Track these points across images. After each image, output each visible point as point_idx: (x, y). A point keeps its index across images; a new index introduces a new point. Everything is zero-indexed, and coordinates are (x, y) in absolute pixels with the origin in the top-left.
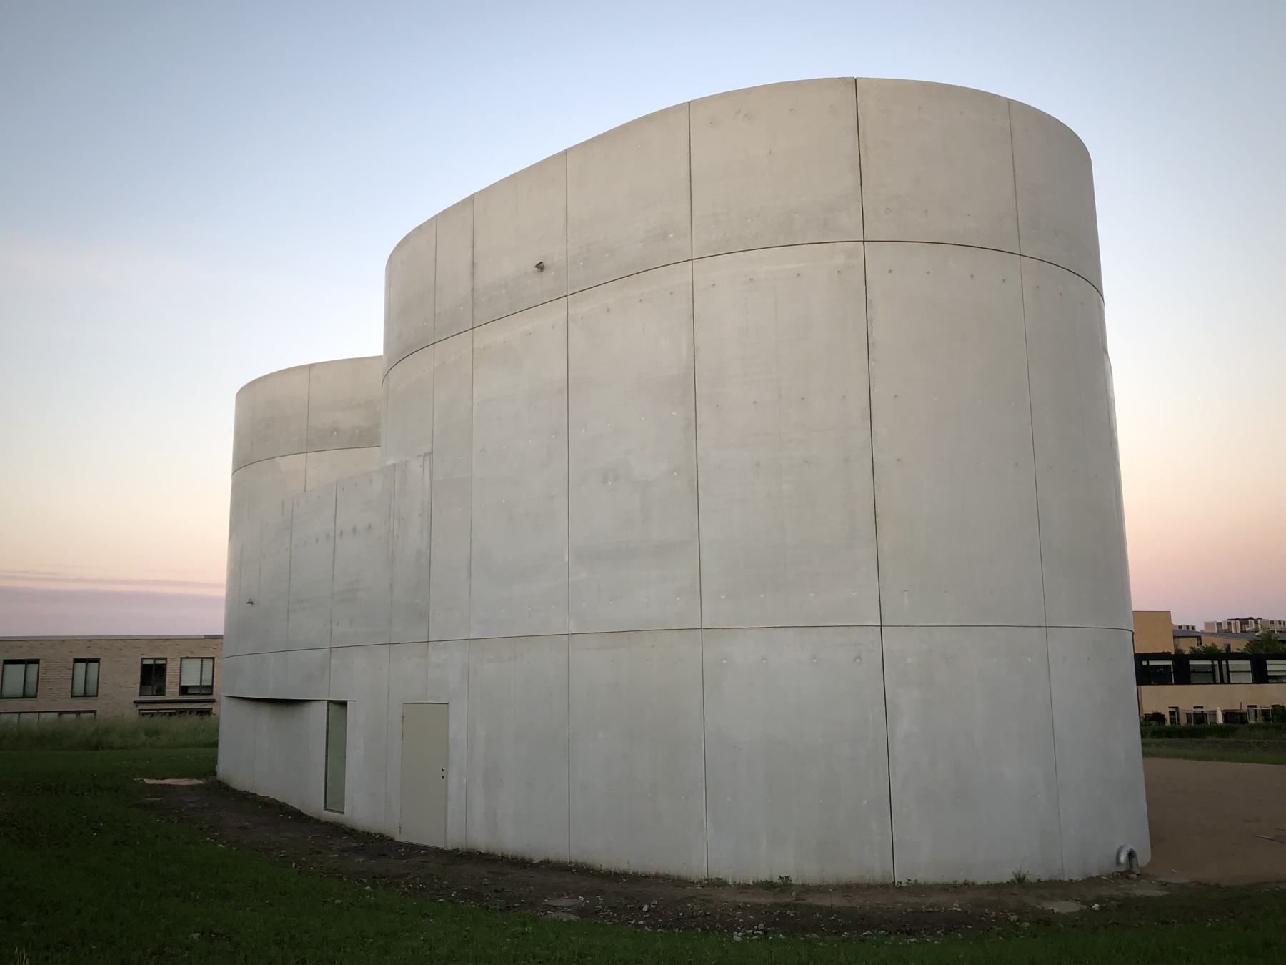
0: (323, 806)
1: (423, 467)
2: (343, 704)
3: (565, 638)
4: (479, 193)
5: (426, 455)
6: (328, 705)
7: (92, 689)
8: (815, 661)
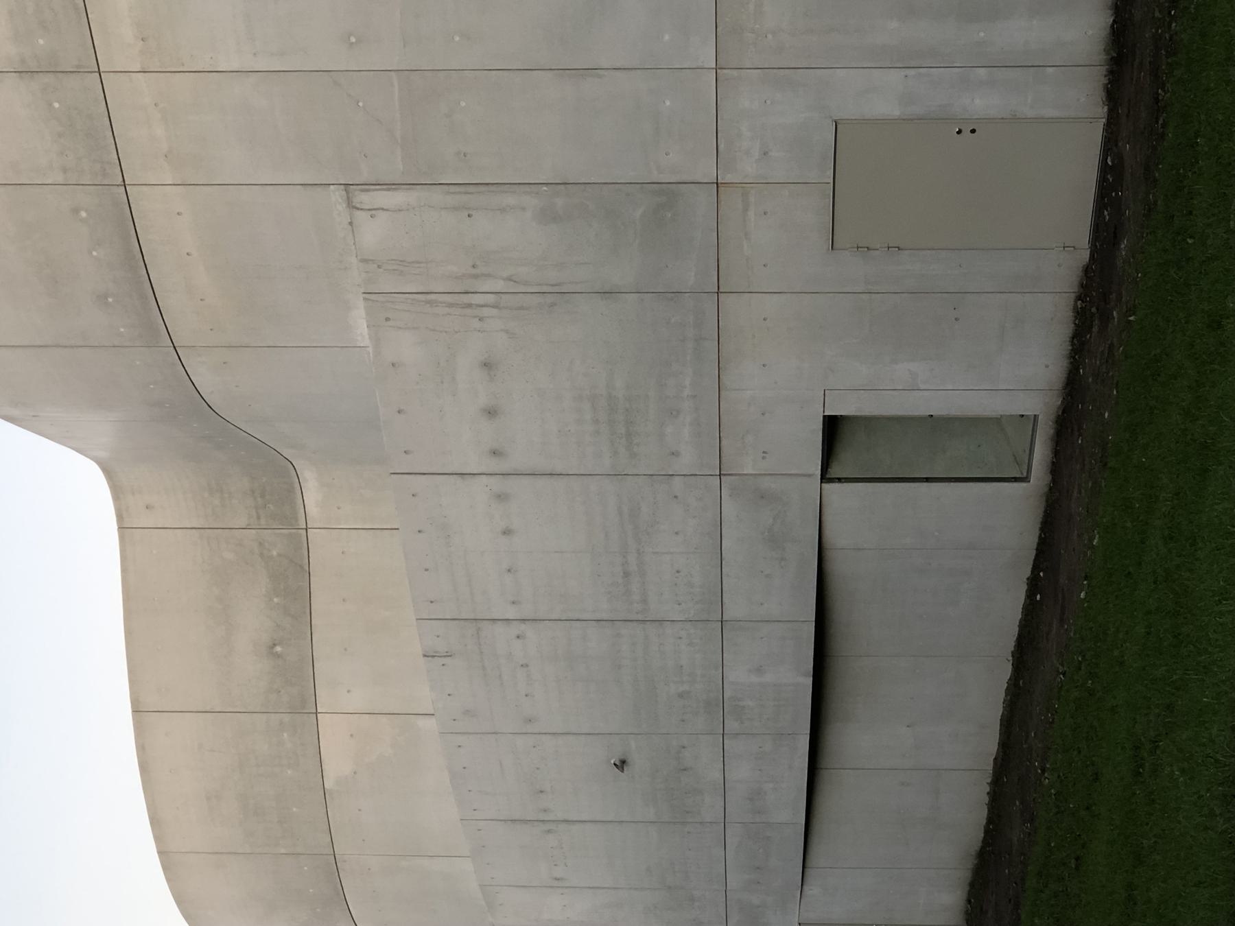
0: (1024, 485)
2: (833, 427)
5: (351, 206)
6: (831, 480)
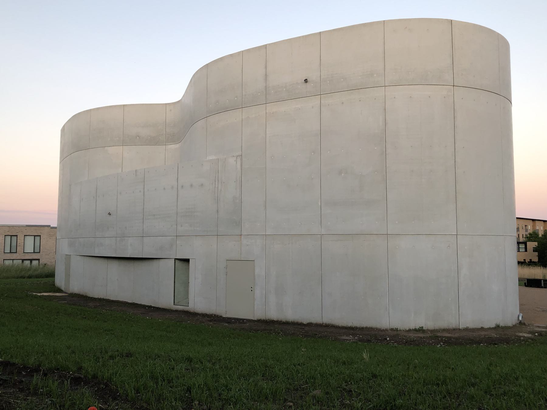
1: (236, 161)
2: (187, 261)
4: (269, 44)
5: (237, 156)
6: (175, 261)
7: (14, 250)
8: (433, 247)
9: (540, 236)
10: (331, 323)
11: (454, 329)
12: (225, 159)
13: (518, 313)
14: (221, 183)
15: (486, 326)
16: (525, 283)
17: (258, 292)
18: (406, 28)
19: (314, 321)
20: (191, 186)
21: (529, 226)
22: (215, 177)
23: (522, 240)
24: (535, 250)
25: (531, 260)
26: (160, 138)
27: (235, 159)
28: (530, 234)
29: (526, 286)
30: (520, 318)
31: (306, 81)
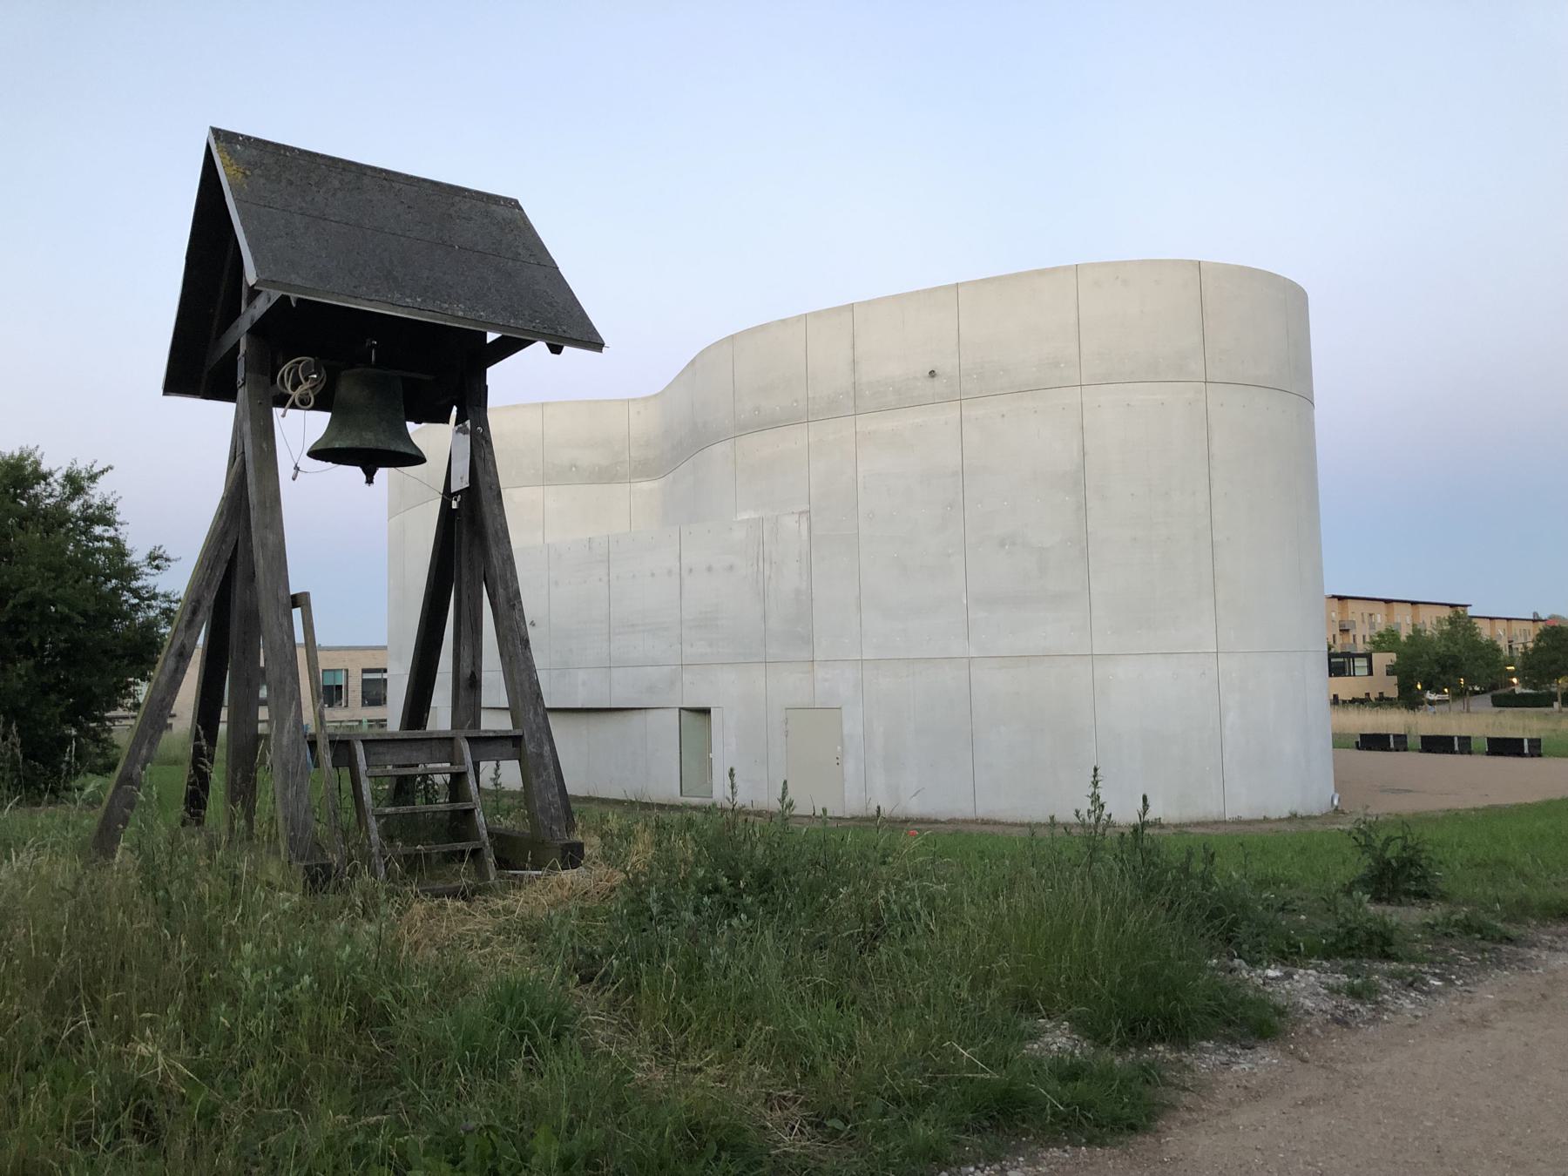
2: (706, 712)
3: (964, 660)
4: (859, 303)
5: (800, 513)
6: (680, 712)
9: (1403, 638)
10: (993, 818)
11: (1216, 822)
12: (777, 517)
13: (1332, 792)
14: (771, 563)
15: (1274, 815)
16: (1357, 743)
17: (850, 767)
18: (1117, 278)
19: (958, 815)
20: (710, 569)
21: (1379, 616)
22: (758, 553)
23: (1362, 648)
24: (1391, 671)
25: (1381, 693)
26: (618, 468)
27: (797, 519)
28: (1380, 635)
29: (1358, 748)
30: (1336, 802)
31: (932, 374)
